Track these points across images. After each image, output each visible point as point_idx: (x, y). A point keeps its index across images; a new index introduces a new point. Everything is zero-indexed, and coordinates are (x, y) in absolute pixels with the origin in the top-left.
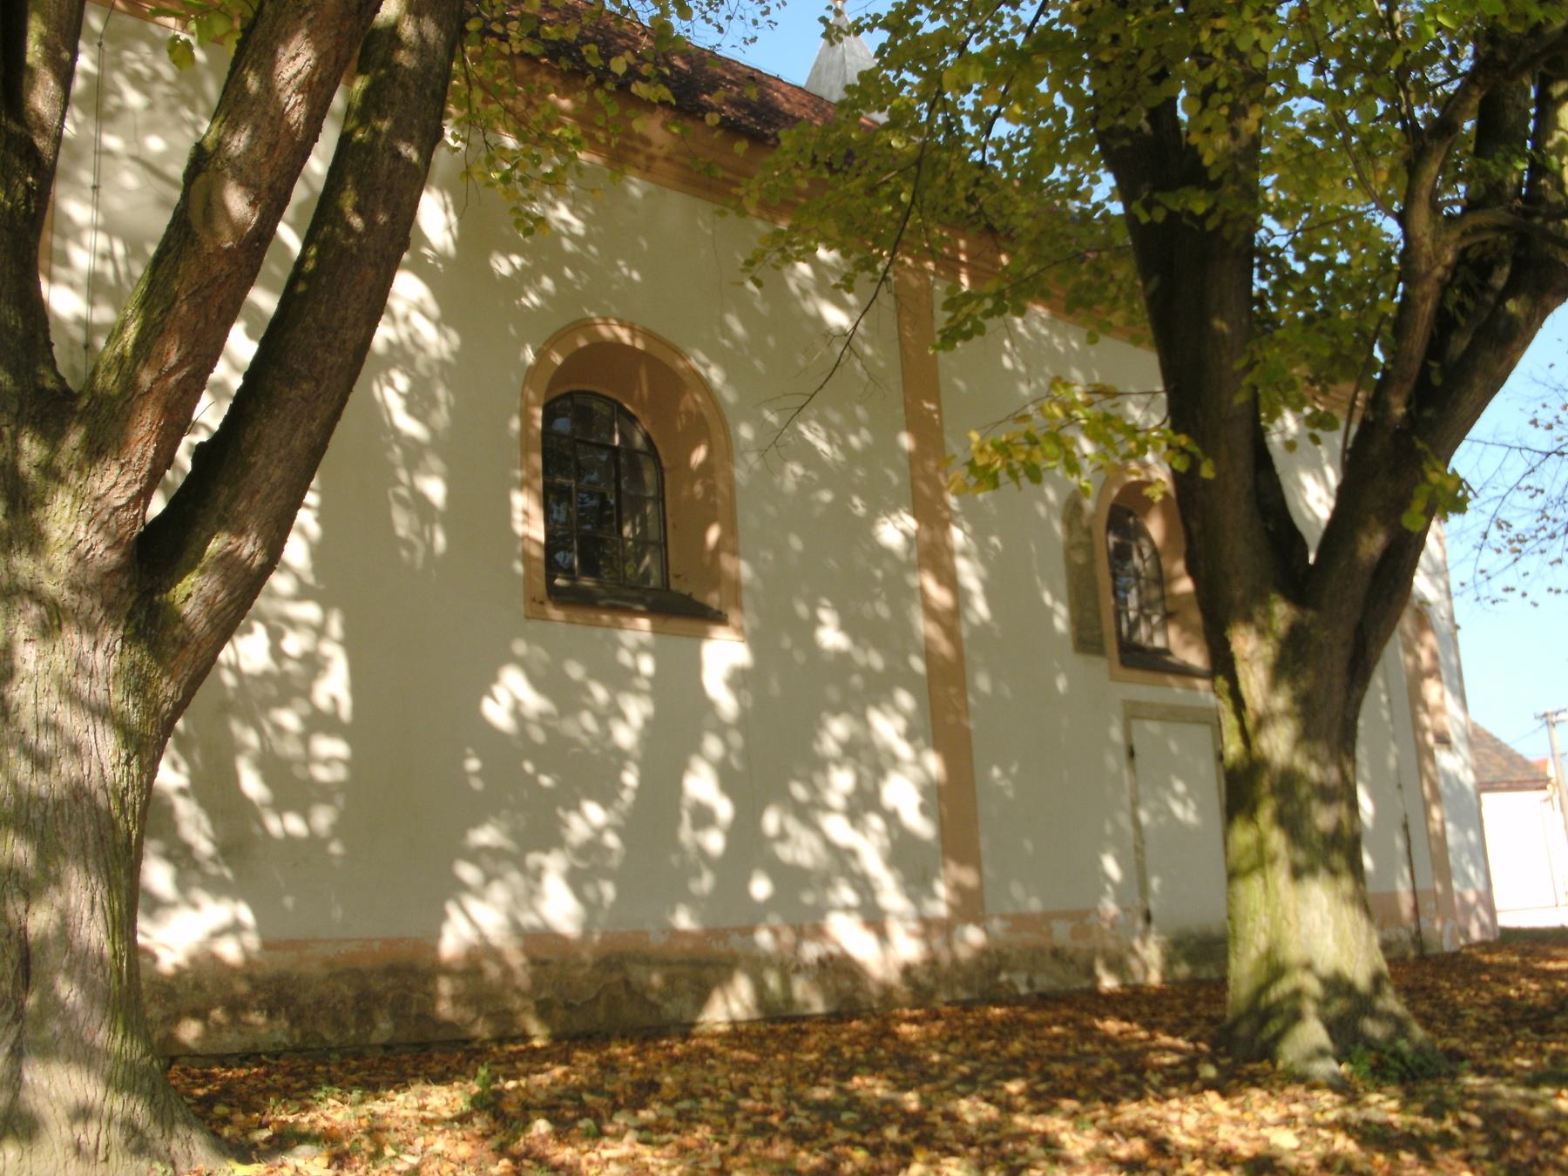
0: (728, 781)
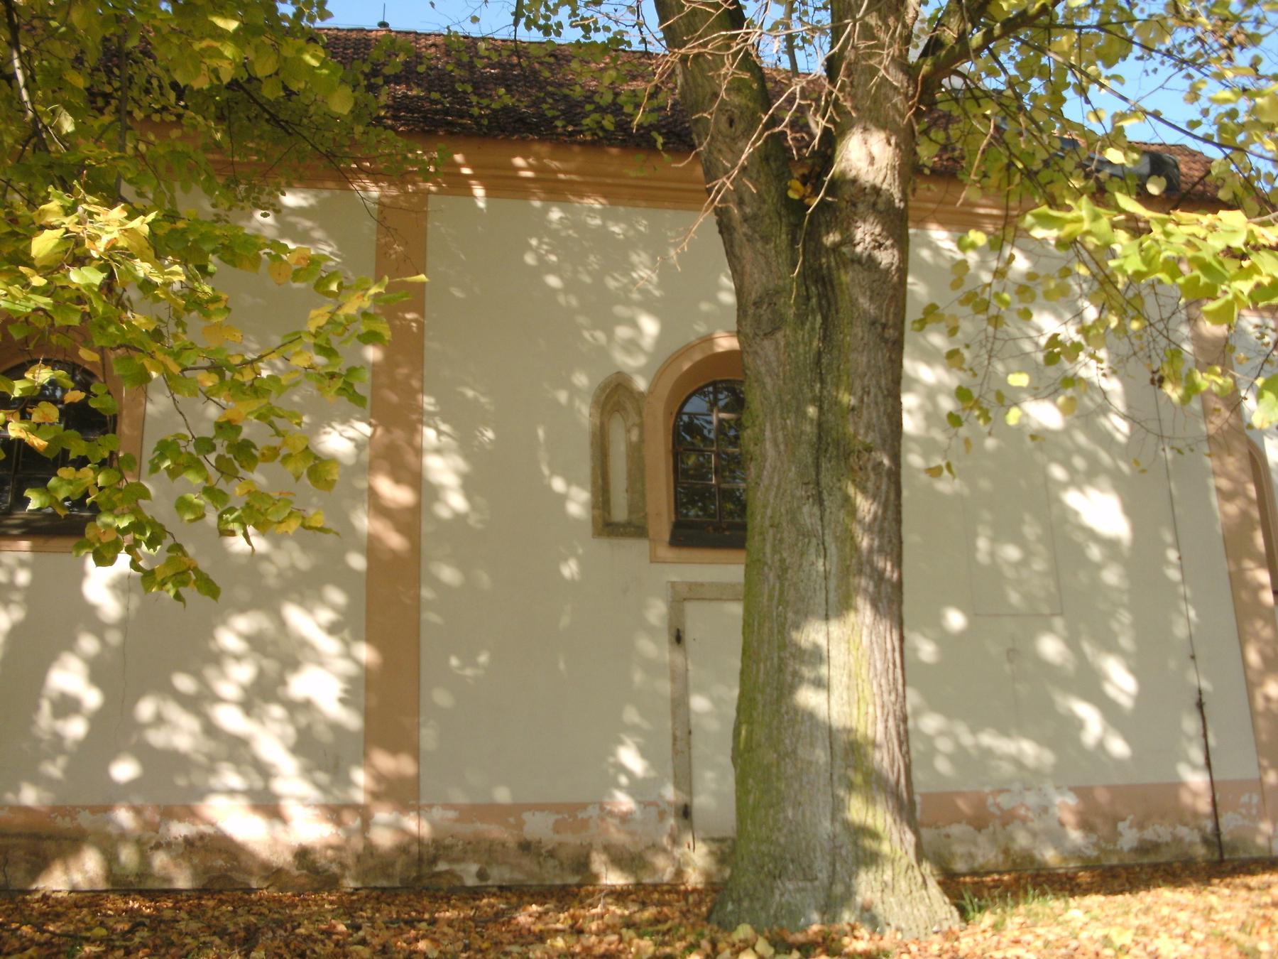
0: (97, 674)
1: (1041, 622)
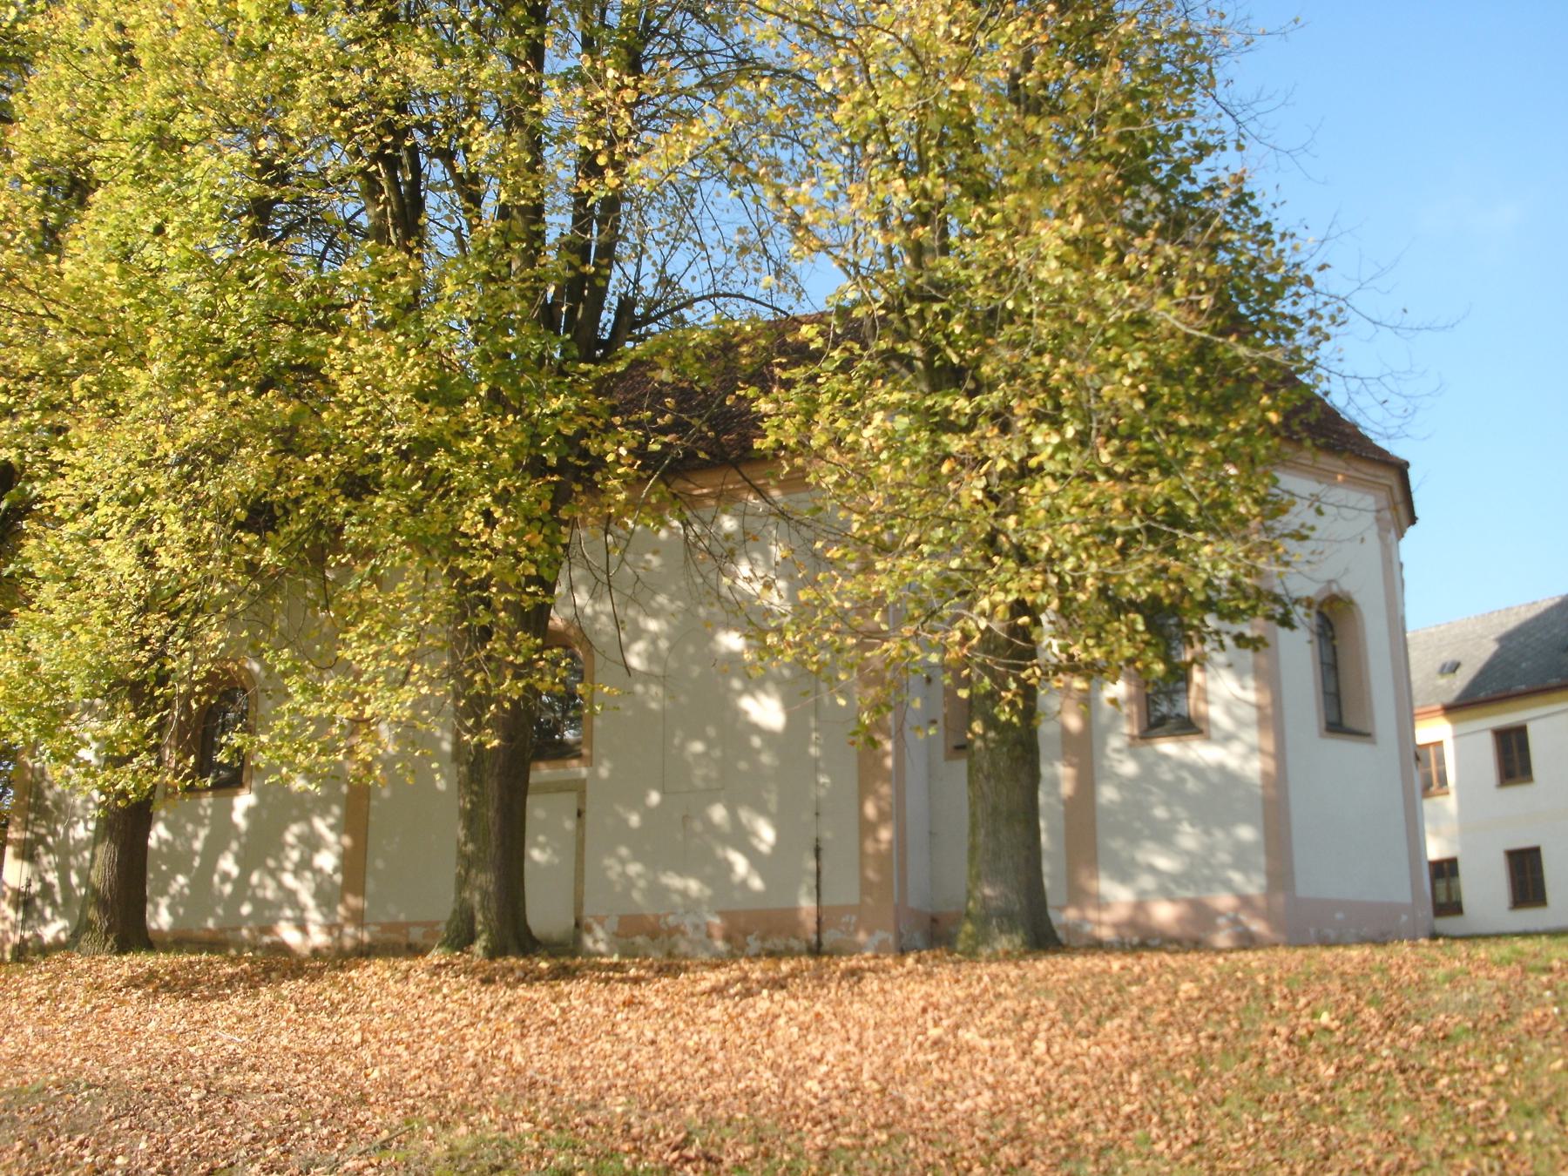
0: (239, 860)
1: (712, 795)
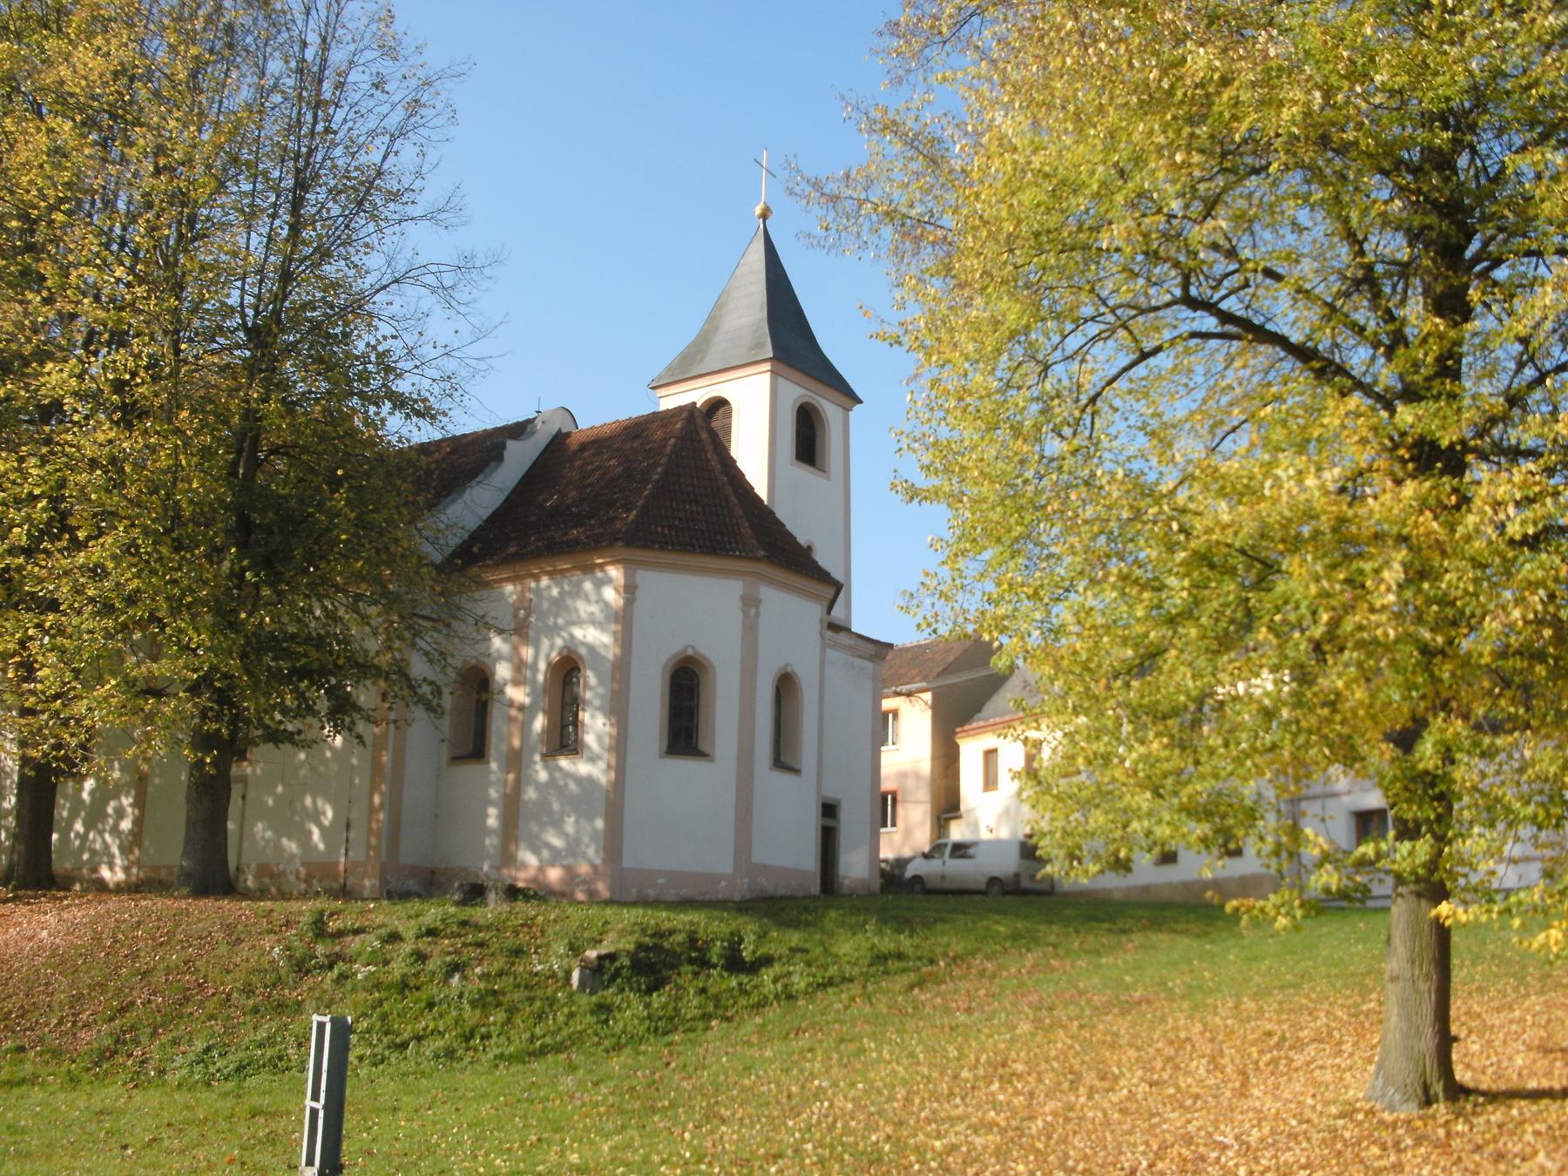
0: (85, 824)
